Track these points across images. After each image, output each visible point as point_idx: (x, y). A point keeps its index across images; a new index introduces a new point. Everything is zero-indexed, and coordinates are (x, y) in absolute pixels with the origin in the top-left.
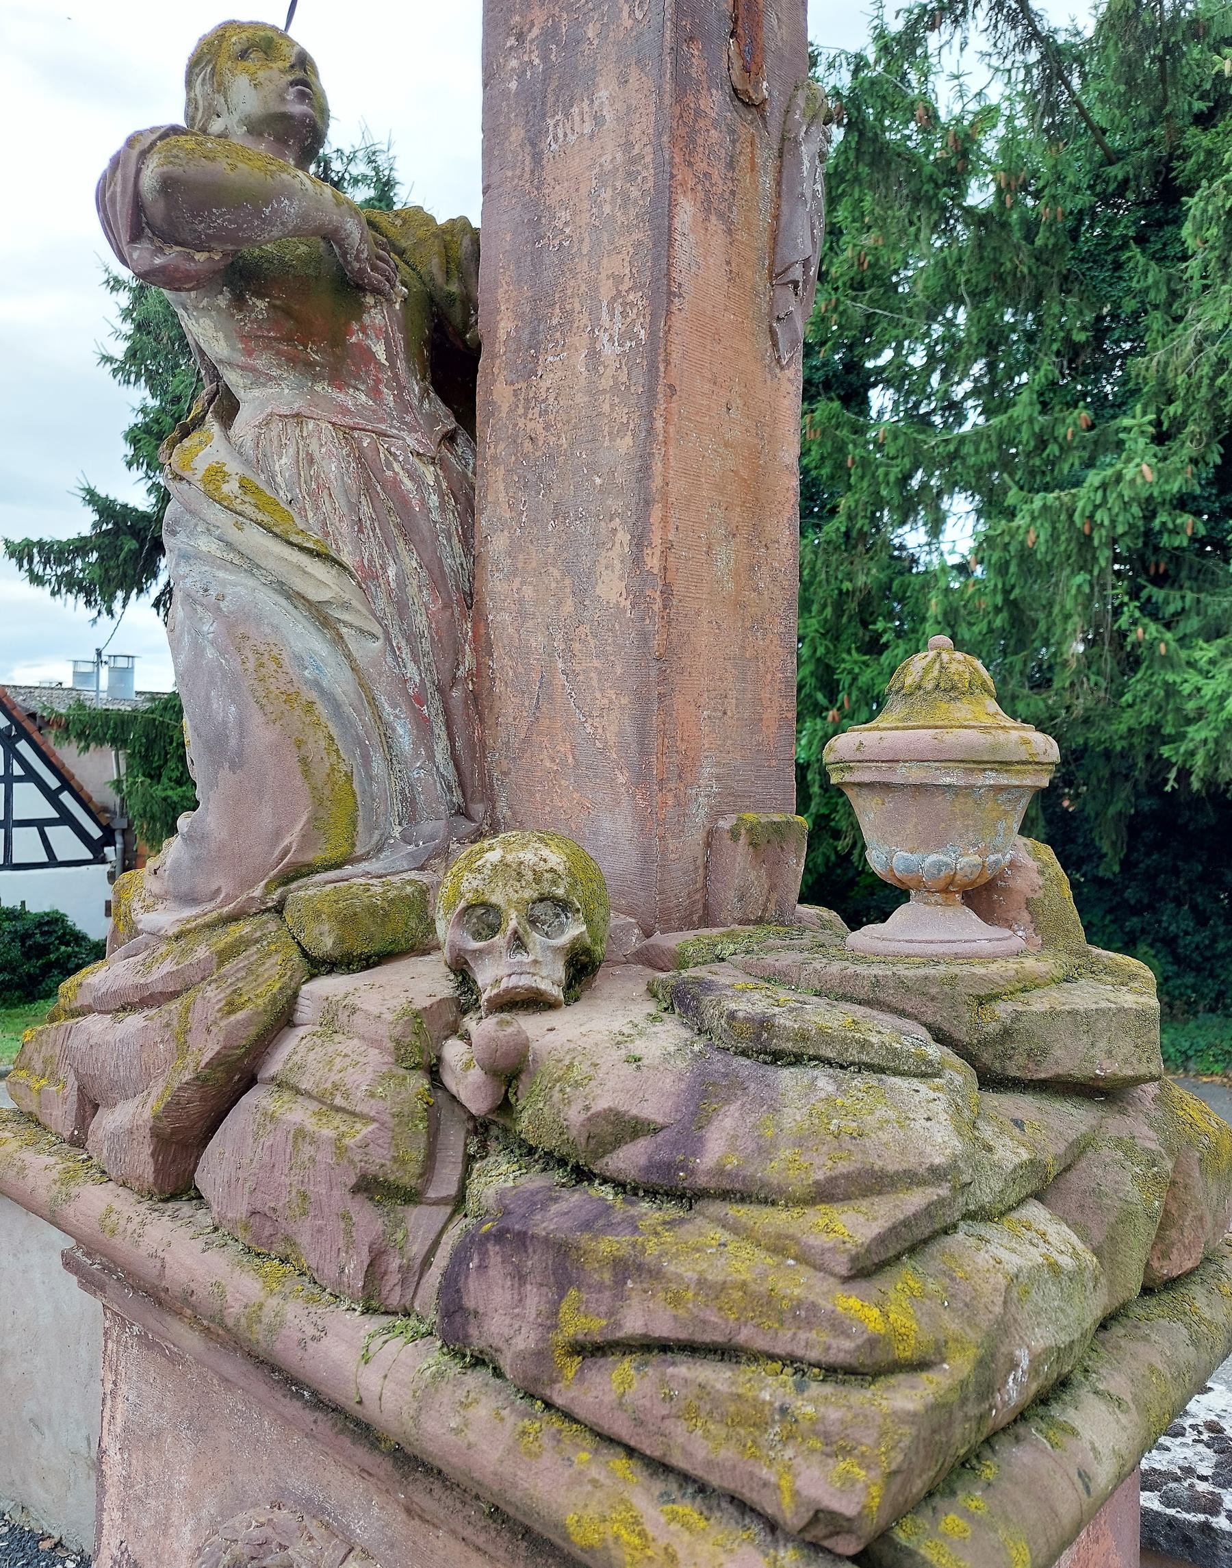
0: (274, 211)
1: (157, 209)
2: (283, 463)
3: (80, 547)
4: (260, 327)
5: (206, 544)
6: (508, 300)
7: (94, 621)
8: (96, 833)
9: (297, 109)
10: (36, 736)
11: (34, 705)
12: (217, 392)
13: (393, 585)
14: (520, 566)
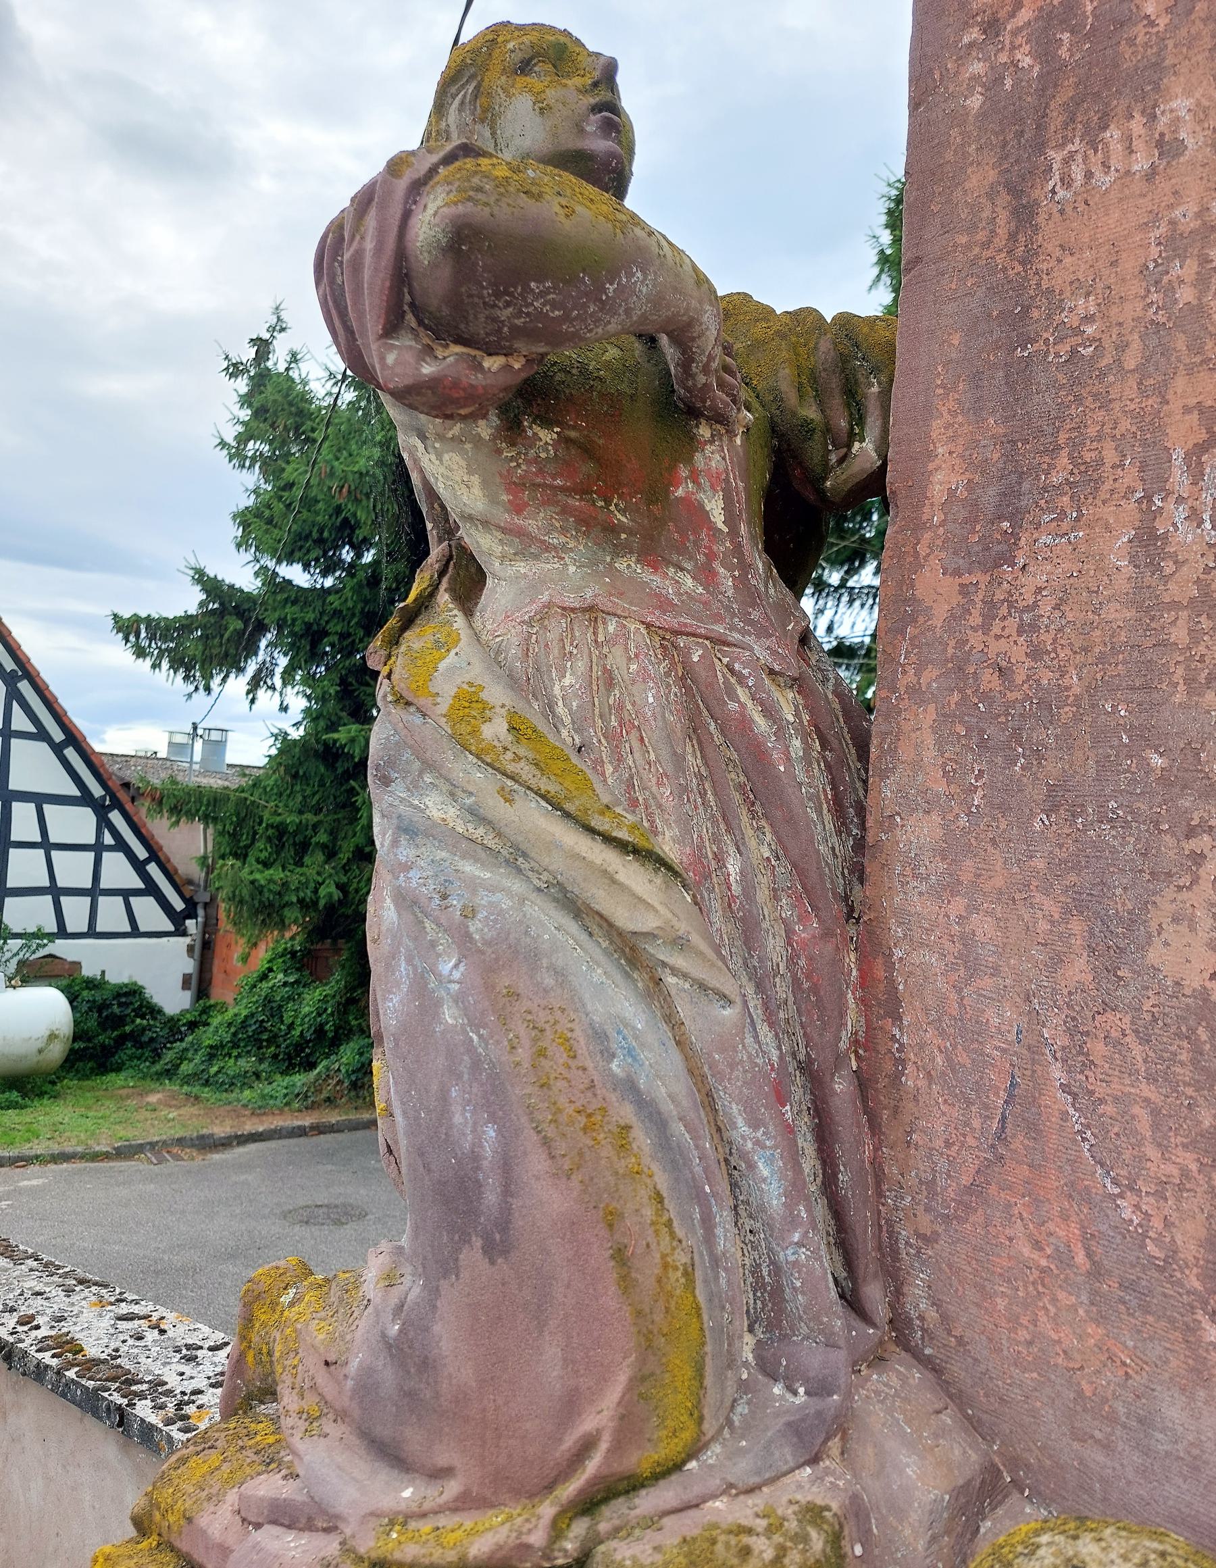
0: (621, 289)
1: (435, 282)
2: (566, 684)
3: (185, 624)
4: (540, 471)
5: (436, 807)
6: (952, 439)
7: (190, 696)
8: (179, 905)
9: (601, 145)
10: (128, 807)
11: (131, 775)
12: (450, 558)
13: (736, 889)
14: (966, 877)
